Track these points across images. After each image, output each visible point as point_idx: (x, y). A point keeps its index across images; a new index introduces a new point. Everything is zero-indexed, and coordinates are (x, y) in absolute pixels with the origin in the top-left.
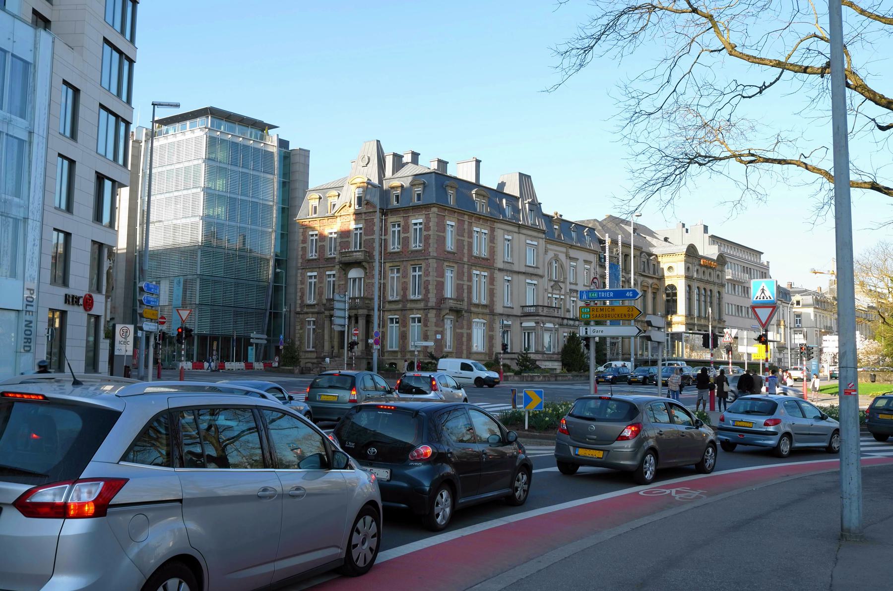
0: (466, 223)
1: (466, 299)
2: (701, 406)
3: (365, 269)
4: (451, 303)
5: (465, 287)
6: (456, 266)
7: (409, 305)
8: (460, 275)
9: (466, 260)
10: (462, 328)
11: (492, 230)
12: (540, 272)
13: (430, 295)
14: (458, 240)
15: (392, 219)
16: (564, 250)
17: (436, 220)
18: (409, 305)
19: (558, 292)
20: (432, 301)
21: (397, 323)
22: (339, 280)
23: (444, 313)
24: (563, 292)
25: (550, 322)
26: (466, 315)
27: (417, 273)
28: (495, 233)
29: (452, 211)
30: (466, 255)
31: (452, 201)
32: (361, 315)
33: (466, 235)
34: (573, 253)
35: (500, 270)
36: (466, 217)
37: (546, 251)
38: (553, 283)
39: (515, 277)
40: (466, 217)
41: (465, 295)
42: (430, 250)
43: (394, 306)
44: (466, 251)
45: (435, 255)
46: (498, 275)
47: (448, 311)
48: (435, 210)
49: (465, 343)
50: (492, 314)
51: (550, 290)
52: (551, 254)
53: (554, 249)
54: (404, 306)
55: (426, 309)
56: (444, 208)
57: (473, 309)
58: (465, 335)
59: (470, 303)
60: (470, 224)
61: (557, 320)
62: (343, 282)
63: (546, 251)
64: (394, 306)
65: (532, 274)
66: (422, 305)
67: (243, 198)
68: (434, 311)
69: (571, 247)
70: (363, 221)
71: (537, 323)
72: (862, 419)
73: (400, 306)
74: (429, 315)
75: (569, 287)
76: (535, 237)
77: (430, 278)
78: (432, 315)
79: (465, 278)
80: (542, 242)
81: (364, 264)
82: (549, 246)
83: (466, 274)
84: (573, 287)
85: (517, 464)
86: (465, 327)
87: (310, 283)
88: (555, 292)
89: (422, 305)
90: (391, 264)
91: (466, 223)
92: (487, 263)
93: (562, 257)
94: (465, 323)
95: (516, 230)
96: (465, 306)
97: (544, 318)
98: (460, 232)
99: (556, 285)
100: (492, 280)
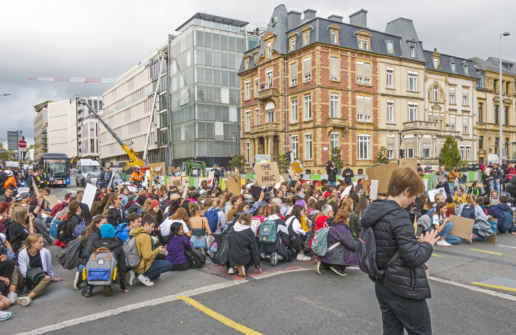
0: (349, 58)
1: (350, 119)
2: (19, 199)
3: (274, 102)
4: (336, 122)
5: (350, 109)
6: (340, 92)
7: (304, 126)
8: (344, 100)
9: (349, 87)
10: (347, 141)
11: (375, 63)
12: (421, 96)
13: (317, 117)
14: (342, 72)
15: (291, 61)
16: (444, 78)
17: (320, 56)
18: (304, 126)
19: (438, 111)
20: (319, 121)
21: (297, 140)
22: (261, 113)
23: (329, 130)
24: (443, 111)
25: (428, 134)
26: (350, 131)
27: (309, 101)
28: (378, 66)
29: (335, 48)
30: (350, 84)
31: (336, 41)
32: (270, 136)
33: (349, 68)
34: (451, 80)
35: (382, 95)
36: (349, 54)
37: (426, 80)
38: (433, 104)
39: (398, 100)
40: (349, 54)
41: (350, 115)
42: (316, 80)
43: (294, 128)
44: (349, 81)
45: (320, 84)
46: (380, 99)
47: (332, 128)
48: (318, 48)
49: (351, 153)
50: (376, 130)
51: (430, 110)
52: (430, 82)
53: (433, 78)
54: (131, 87)
55: (314, 128)
56: (327, 45)
57: (358, 126)
58: (351, 147)
59: (354, 122)
60: (353, 59)
61: (434, 132)
62: (263, 114)
63: (426, 80)
64: (294, 128)
65: (413, 98)
66: (311, 125)
67: (224, 69)
68: (321, 129)
69: (451, 75)
70: (272, 67)
71: (415, 135)
72: (395, 179)
73: (298, 127)
74: (317, 132)
75: (448, 107)
76: (416, 68)
77: (316, 103)
78: (319, 131)
79: (350, 102)
80: (422, 72)
81: (272, 98)
82: (429, 75)
83: (350, 99)
84: (453, 107)
85: (248, 281)
86: (351, 140)
87: (248, 117)
88: (435, 111)
89: (311, 125)
90: (291, 97)
91: (349, 58)
92: (371, 90)
93: (442, 84)
94: (350, 137)
95: (398, 63)
96: (350, 123)
97: (422, 131)
98: (344, 65)
99: (437, 105)
100: (375, 103)
